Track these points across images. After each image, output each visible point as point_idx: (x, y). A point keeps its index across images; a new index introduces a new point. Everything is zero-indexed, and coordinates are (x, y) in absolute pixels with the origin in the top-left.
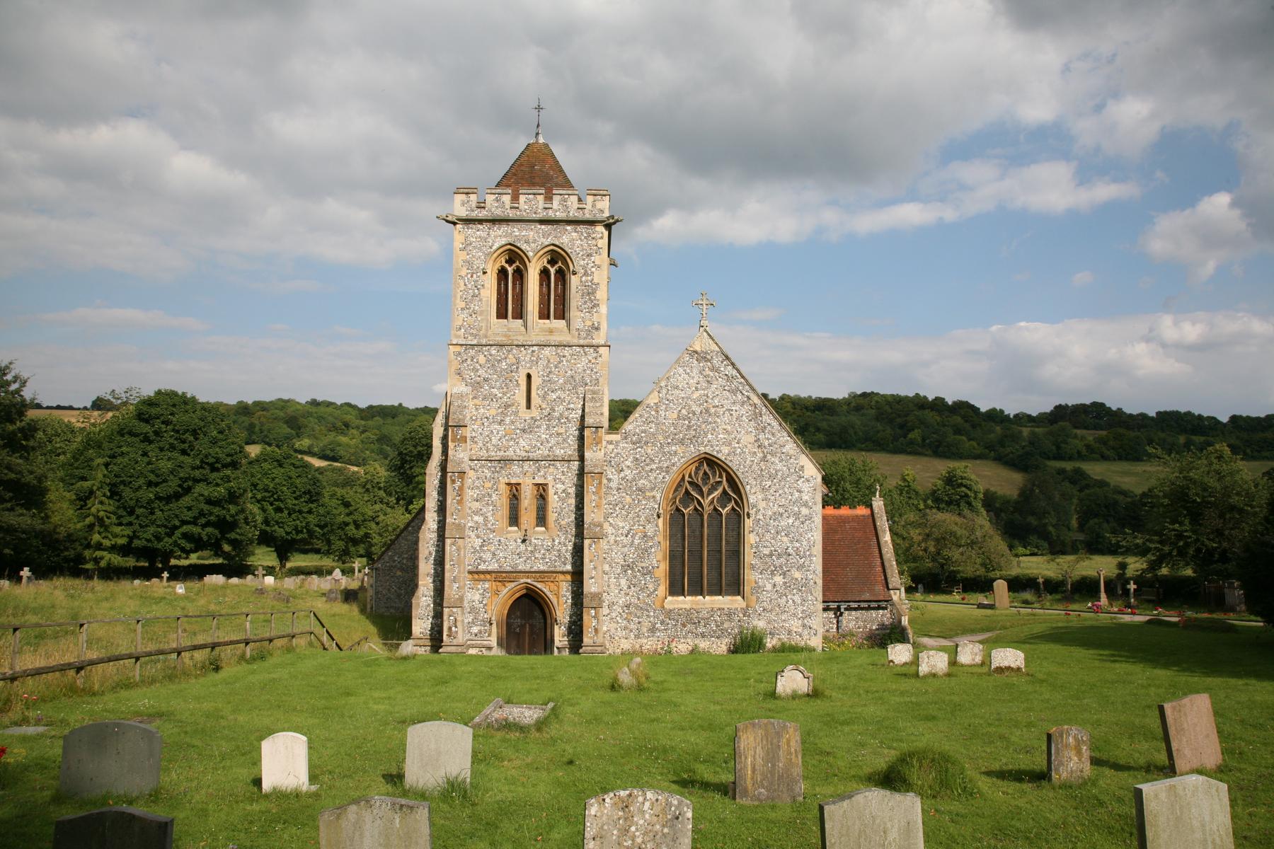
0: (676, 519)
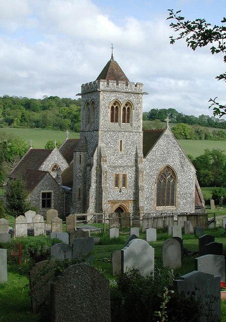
0: (159, 183)
